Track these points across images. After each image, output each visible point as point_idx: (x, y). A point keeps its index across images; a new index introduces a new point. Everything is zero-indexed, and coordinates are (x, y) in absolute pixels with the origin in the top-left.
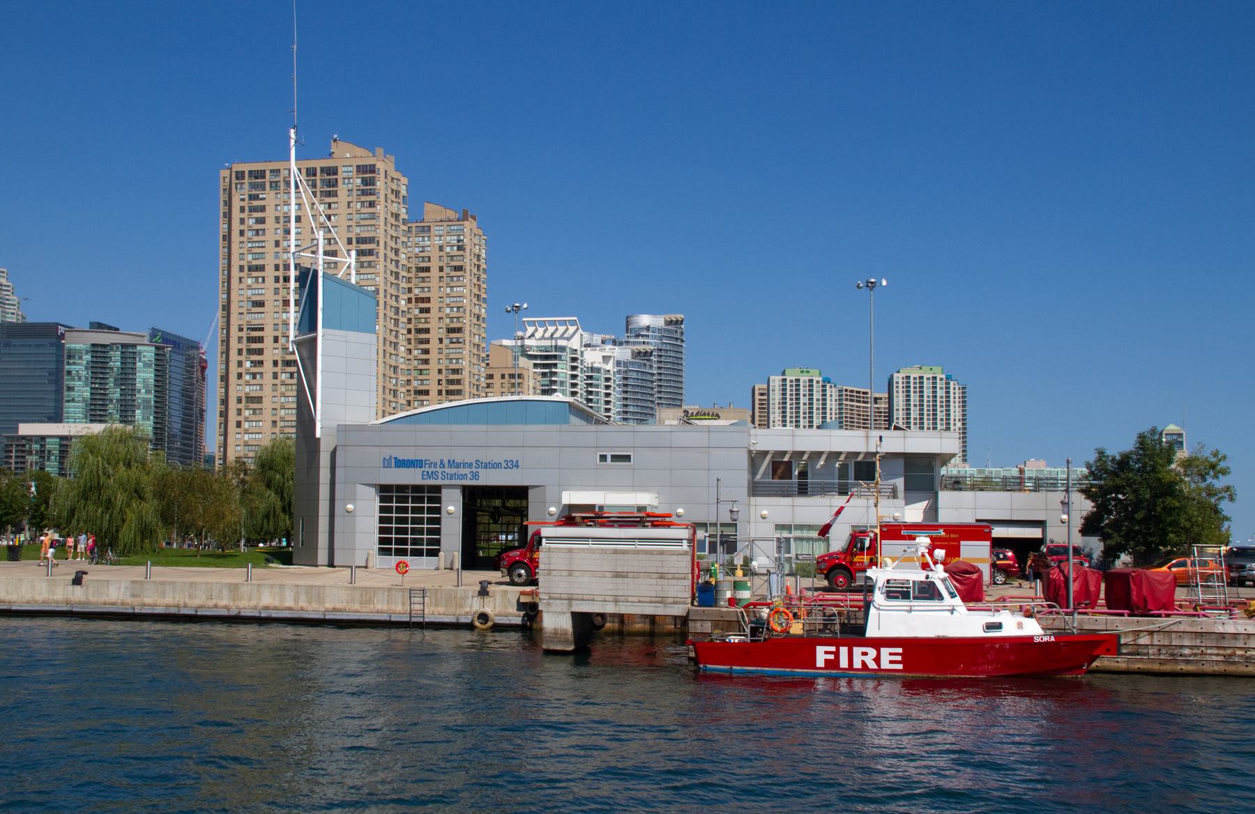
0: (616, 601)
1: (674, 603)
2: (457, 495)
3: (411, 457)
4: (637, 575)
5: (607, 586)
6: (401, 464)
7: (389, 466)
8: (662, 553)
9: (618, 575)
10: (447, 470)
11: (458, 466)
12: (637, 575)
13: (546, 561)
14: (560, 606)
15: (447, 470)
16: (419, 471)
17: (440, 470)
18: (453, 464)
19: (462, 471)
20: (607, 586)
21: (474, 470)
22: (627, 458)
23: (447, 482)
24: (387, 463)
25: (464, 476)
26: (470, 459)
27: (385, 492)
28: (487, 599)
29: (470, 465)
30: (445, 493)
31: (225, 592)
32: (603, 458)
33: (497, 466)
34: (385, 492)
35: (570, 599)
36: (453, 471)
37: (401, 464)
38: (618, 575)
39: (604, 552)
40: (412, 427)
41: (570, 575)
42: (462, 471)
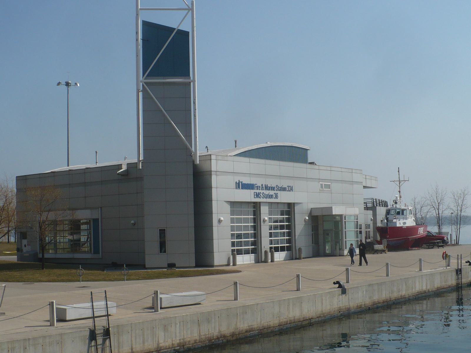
15: (265, 191)
16: (253, 191)
18: (267, 188)
21: (276, 192)
23: (264, 200)
26: (271, 183)
34: (233, 204)
36: (267, 192)
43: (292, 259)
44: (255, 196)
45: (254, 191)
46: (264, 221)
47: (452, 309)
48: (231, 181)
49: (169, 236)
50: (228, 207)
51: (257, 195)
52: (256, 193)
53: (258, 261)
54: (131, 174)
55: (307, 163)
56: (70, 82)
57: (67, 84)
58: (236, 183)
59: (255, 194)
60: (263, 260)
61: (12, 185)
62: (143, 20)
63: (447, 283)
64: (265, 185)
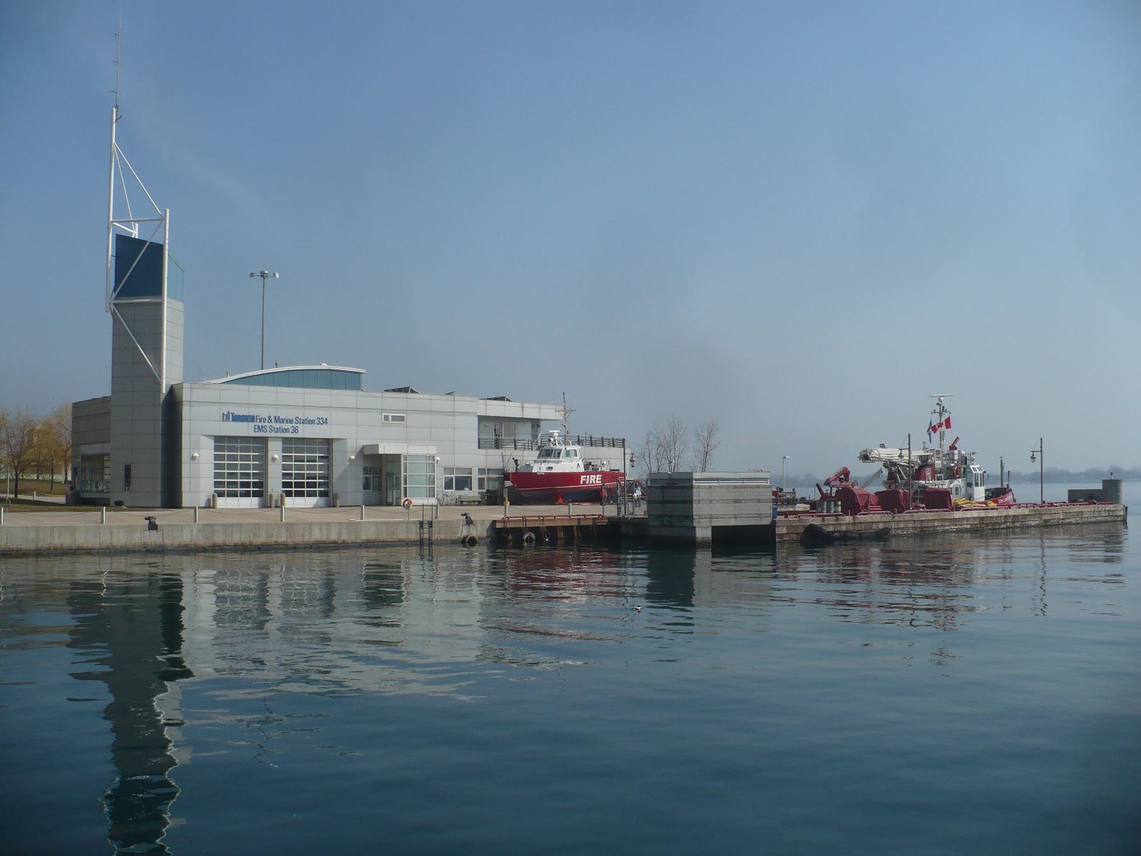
0: (736, 518)
1: (765, 517)
2: (279, 445)
3: (245, 413)
4: (746, 501)
5: (731, 509)
6: (237, 418)
7: (228, 419)
8: (758, 487)
9: (736, 501)
10: (274, 425)
11: (282, 421)
12: (746, 501)
13: (697, 494)
14: (706, 522)
15: (274, 425)
16: (252, 424)
17: (268, 425)
18: (277, 420)
19: (285, 426)
20: (731, 509)
21: (295, 425)
22: (402, 419)
23: (273, 434)
24: (226, 417)
25: (287, 430)
26: (291, 414)
27: (219, 440)
28: (472, 527)
29: (291, 421)
30: (271, 444)
31: (284, 531)
32: (386, 418)
33: (311, 422)
34: (219, 440)
35: (711, 518)
36: (278, 425)
37: (237, 418)
38: (736, 501)
39: (729, 487)
40: (245, 387)
41: (699, 503)
42: (285, 426)
43: (330, 507)
44: (256, 430)
45: (255, 423)
46: (274, 459)
47: (448, 570)
48: (216, 412)
49: (134, 473)
50: (211, 443)
51: (260, 429)
52: (259, 426)
53: (264, 505)
54: (105, 400)
55: (408, 392)
56: (266, 272)
57: (263, 275)
58: (223, 414)
59: (256, 427)
60: (212, 506)
61: (71, 405)
62: (118, 233)
63: (410, 536)
64: (275, 417)
